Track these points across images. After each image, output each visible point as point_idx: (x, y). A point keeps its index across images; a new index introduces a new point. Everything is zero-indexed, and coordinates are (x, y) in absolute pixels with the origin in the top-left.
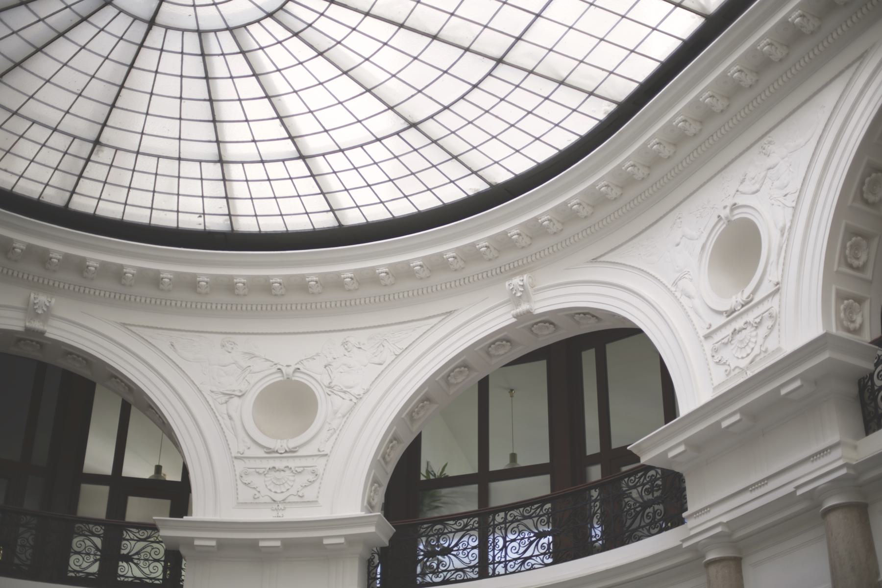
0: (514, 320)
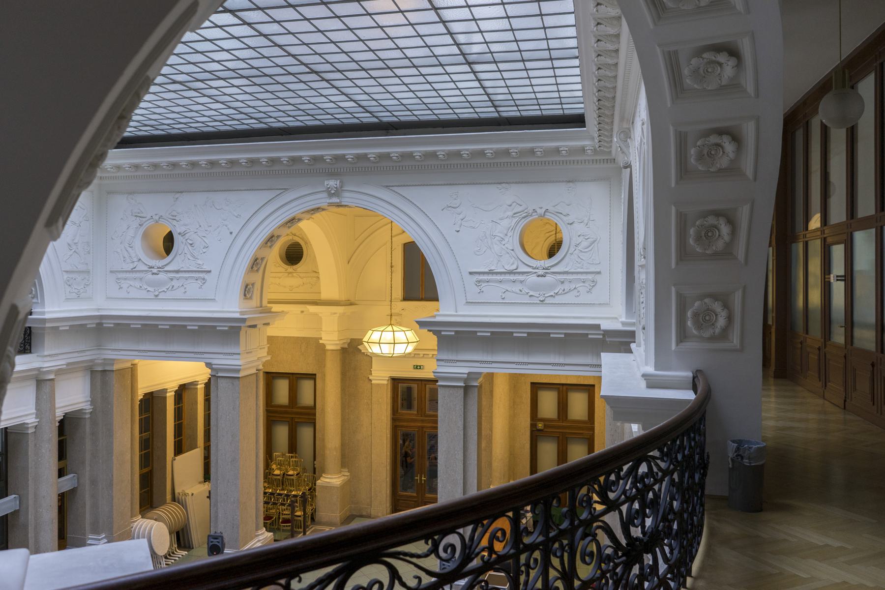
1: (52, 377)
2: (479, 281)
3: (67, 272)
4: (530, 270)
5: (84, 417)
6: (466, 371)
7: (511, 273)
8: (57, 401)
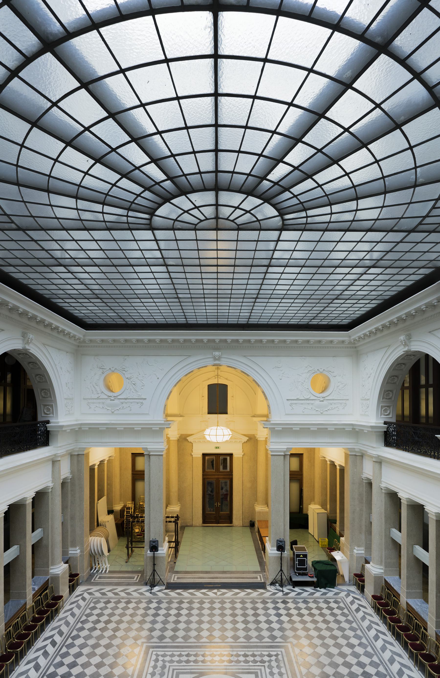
1: (59, 459)
2: (292, 404)
3: (66, 399)
4: (316, 398)
5: (67, 481)
6: (286, 447)
7: (307, 399)
8: (62, 472)
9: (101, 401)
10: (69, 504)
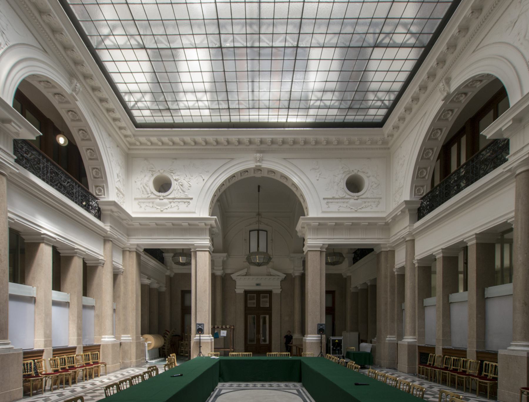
0: (444, 101)
9: (151, 200)
10: (122, 294)
